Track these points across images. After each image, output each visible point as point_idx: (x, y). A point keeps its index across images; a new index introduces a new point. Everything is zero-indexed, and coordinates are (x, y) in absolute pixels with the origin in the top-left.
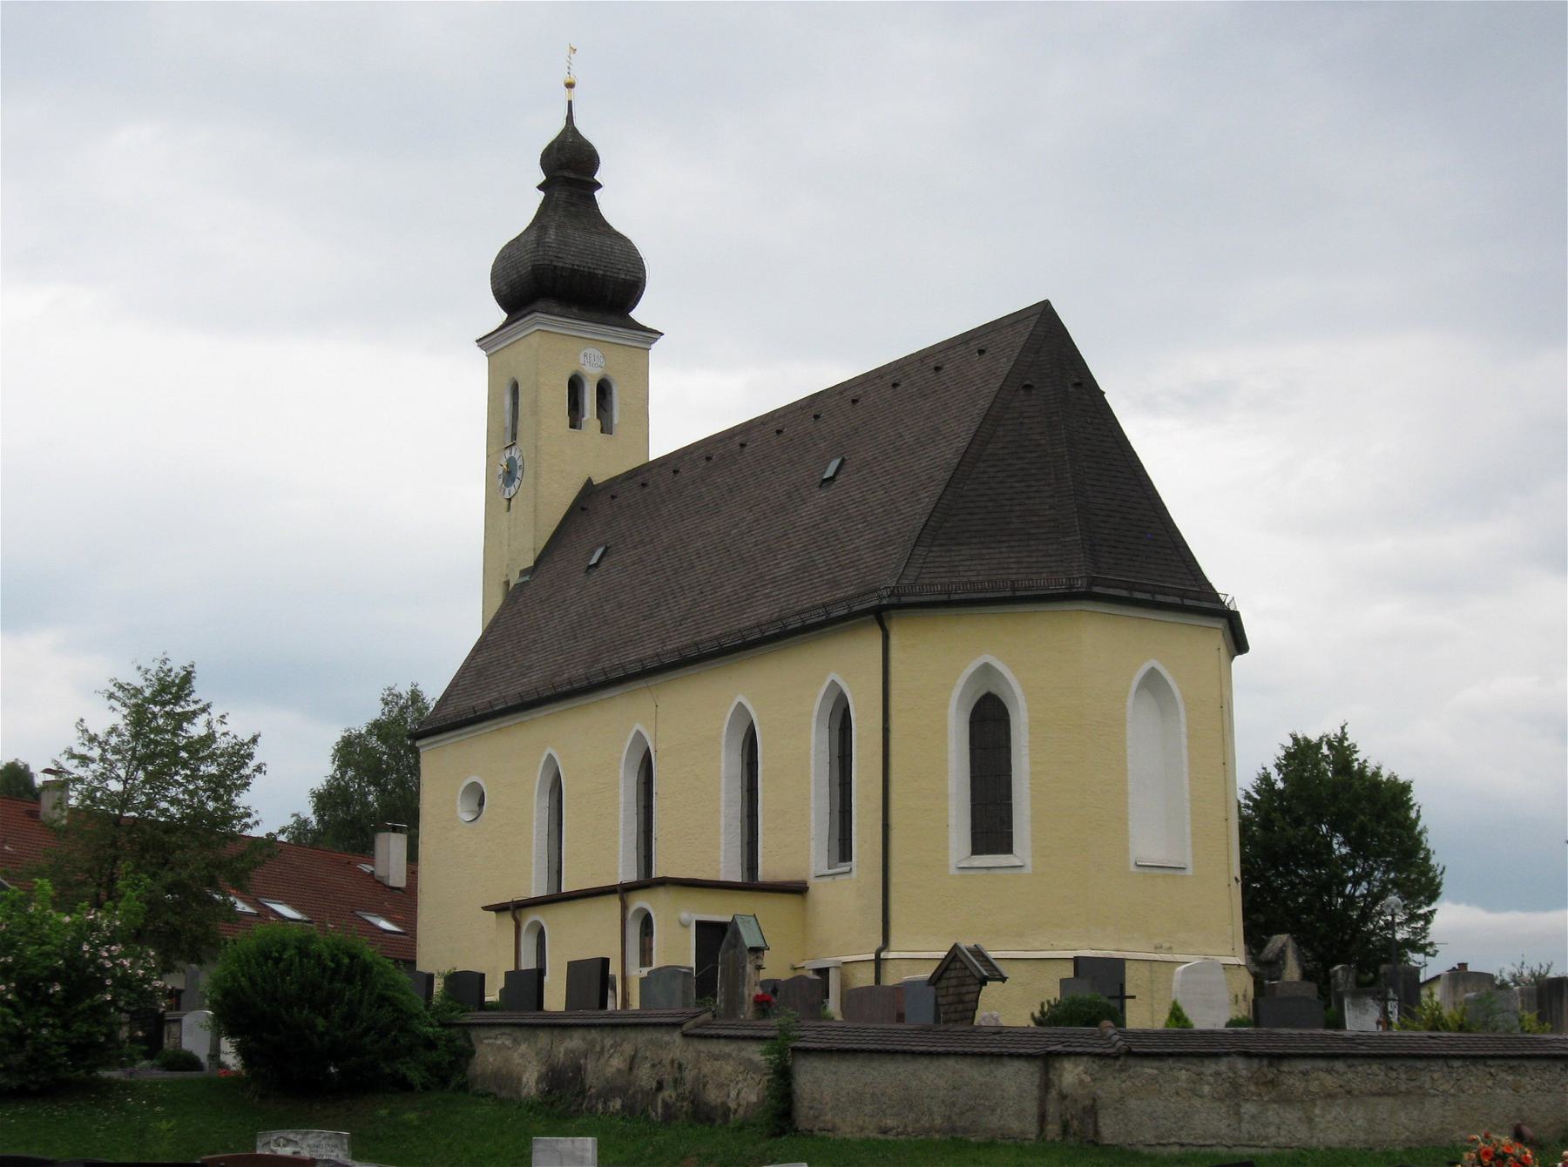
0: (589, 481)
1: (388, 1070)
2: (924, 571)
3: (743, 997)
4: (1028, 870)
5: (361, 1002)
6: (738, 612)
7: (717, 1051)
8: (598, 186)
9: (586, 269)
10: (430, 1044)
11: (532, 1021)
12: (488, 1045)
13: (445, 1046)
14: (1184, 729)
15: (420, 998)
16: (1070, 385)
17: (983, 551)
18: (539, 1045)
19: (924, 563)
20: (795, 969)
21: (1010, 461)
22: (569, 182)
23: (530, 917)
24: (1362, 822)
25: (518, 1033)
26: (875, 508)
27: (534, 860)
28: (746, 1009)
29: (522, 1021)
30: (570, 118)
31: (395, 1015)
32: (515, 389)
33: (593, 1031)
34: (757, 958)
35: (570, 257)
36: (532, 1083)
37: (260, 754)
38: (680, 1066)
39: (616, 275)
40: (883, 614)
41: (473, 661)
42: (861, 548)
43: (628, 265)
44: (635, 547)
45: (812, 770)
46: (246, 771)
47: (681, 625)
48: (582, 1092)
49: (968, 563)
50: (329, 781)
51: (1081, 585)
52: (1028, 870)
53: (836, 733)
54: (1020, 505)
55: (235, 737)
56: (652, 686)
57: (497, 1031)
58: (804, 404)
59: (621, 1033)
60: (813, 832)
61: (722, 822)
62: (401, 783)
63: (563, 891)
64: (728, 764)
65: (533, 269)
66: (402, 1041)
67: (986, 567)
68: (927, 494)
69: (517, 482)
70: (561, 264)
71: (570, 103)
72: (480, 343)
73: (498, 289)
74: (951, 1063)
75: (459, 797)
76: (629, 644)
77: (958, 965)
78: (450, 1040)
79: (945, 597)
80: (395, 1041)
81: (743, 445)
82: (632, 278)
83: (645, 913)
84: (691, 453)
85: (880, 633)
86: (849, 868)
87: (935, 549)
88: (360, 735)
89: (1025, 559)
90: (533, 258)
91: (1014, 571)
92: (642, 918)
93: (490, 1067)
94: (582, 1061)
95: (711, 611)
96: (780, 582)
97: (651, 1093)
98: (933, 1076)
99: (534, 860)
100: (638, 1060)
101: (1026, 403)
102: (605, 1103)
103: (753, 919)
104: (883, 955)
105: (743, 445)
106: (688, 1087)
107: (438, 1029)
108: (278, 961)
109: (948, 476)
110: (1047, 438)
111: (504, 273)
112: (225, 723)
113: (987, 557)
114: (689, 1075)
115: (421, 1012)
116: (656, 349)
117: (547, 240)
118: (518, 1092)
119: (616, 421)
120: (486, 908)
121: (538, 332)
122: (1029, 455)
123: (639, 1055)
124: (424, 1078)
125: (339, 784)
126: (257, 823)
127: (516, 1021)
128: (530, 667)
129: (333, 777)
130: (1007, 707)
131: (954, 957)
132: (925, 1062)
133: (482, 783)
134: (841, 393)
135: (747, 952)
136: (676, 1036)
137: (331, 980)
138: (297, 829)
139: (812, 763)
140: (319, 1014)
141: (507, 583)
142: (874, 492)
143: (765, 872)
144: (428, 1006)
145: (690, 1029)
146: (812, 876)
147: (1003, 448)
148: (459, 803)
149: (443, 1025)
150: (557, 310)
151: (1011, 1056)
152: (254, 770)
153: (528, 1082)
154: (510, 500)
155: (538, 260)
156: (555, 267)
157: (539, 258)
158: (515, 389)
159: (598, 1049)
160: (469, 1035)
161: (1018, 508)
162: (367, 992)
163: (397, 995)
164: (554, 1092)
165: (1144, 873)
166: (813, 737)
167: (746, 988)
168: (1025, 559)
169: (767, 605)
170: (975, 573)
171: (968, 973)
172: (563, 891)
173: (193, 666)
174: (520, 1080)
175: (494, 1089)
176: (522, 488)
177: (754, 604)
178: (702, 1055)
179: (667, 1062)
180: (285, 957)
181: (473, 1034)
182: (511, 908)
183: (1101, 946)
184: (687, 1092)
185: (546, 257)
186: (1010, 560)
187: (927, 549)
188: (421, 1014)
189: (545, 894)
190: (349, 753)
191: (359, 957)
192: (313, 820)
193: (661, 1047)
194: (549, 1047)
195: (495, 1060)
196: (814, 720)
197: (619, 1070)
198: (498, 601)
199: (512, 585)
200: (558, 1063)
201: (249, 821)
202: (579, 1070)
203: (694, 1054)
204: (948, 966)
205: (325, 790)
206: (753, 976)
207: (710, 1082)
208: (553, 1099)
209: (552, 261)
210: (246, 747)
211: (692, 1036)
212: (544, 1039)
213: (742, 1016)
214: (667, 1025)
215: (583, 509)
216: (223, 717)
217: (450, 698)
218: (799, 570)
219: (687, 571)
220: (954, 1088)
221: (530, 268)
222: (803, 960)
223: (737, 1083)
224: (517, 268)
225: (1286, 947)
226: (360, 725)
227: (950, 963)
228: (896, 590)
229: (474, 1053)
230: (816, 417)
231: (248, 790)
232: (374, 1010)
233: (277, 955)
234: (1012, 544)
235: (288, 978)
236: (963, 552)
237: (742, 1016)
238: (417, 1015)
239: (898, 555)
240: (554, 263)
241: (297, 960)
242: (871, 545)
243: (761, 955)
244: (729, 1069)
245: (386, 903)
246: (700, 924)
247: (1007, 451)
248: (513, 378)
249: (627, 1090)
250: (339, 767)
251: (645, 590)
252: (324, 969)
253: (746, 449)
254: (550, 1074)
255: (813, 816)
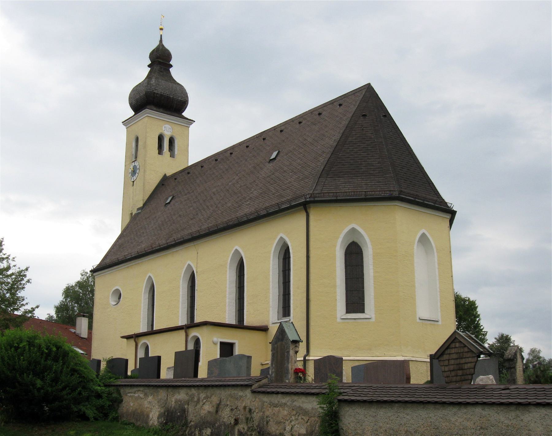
0: (165, 175)
1: (75, 410)
2: (324, 187)
3: (288, 370)
4: (373, 320)
5: (61, 372)
6: (235, 212)
7: (276, 402)
8: (171, 66)
9: (166, 95)
10: (99, 396)
11: (156, 384)
12: (130, 396)
13: (107, 396)
14: (436, 260)
15: (94, 372)
16: (381, 116)
17: (350, 180)
18: (160, 397)
19: (324, 184)
20: (262, 365)
21: (359, 144)
22: (160, 63)
23: (143, 341)
24: (461, 315)
25: (147, 390)
26: (297, 166)
27: (142, 320)
28: (290, 376)
29: (150, 384)
30: (161, 41)
31: (80, 379)
32: (137, 140)
33: (193, 390)
34: (296, 346)
35: (160, 90)
36: (155, 418)
37: (29, 275)
38: (250, 410)
39: (178, 98)
40: (307, 206)
41: (118, 242)
42: (292, 182)
43: (182, 95)
44: (186, 195)
45: (271, 276)
46: (23, 282)
47: (208, 220)
48: (186, 424)
49: (344, 185)
50: (61, 302)
51: (396, 194)
52: (373, 320)
53: (281, 260)
54: (365, 162)
55: (19, 268)
56: (196, 244)
57: (135, 389)
58: (258, 136)
59: (209, 392)
60: (271, 303)
61: (227, 301)
62: (87, 303)
63: (154, 330)
64: (230, 277)
65: (146, 93)
66: (83, 394)
67: (352, 186)
68: (322, 158)
69: (137, 174)
70: (156, 92)
71: (161, 35)
72: (124, 123)
73: (131, 102)
74: (478, 410)
75: (110, 295)
76: (185, 229)
77: (457, 345)
78: (110, 394)
79: (335, 198)
80: (80, 393)
81: (231, 154)
82: (183, 100)
83: (197, 338)
84: (209, 160)
85: (305, 214)
86: (289, 319)
87: (328, 179)
88: (72, 286)
89: (369, 184)
90: (146, 89)
91: (364, 188)
92: (194, 341)
93: (131, 408)
94: (186, 406)
95: (222, 213)
96: (254, 199)
97: (230, 425)
98: (462, 420)
99: (142, 320)
100: (221, 406)
101: (364, 122)
102: (200, 430)
103: (291, 325)
104: (307, 358)
105: (231, 154)
106: (256, 423)
107: (103, 388)
108: (17, 348)
109: (332, 150)
110: (375, 136)
111: (134, 96)
112: (14, 261)
113: (352, 182)
114: (256, 416)
115: (94, 379)
116: (192, 127)
117: (151, 82)
118: (147, 423)
119: (176, 153)
120: (123, 337)
121: (147, 117)
122: (367, 142)
123: (223, 403)
124: (95, 414)
125: (64, 304)
126: (27, 304)
127: (147, 384)
128: (142, 242)
129: (62, 301)
130: (362, 248)
131: (454, 340)
132: (455, 409)
133: (120, 289)
134: (275, 130)
135: (290, 343)
136: (248, 392)
137: (46, 360)
138: (49, 319)
139: (271, 273)
140: (39, 378)
141: (132, 214)
142: (295, 161)
143: (247, 321)
144: (97, 376)
145: (256, 389)
146: (270, 323)
147: (356, 139)
148: (110, 297)
149: (106, 386)
150: (155, 109)
151: (538, 405)
152: (26, 282)
153: (153, 418)
154: (133, 182)
155: (148, 90)
156: (154, 92)
157: (148, 89)
158: (137, 140)
159: (196, 399)
160: (120, 391)
161: (364, 163)
162: (65, 366)
163: (81, 369)
164: (168, 424)
165: (423, 323)
166: (271, 262)
167: (290, 364)
168: (369, 184)
169: (249, 208)
170: (347, 189)
171: (466, 349)
172: (154, 330)
173: (3, 239)
174: (148, 416)
175: (133, 421)
176: (139, 177)
177: (242, 209)
178: (265, 404)
179: (241, 408)
180: (21, 346)
181: (122, 391)
182: (134, 337)
183: (406, 355)
184: (255, 426)
185: (151, 89)
186: (363, 184)
187: (325, 179)
188: (94, 380)
189: (146, 331)
190: (69, 292)
191: (61, 348)
192: (55, 316)
193: (237, 399)
194: (166, 398)
195: (134, 405)
196: (272, 254)
197: (209, 412)
198: (128, 220)
199: (133, 214)
200: (171, 407)
201: (24, 302)
202: (184, 411)
203: (260, 403)
204: (449, 345)
205: (59, 305)
206: (293, 357)
207: (271, 420)
208: (168, 428)
209: (153, 90)
210: (23, 272)
211: (259, 392)
212: (162, 394)
213: (287, 381)
214: (242, 385)
215: (163, 185)
216: (14, 258)
217: (108, 256)
218: (262, 193)
219: (209, 200)
220: (481, 428)
221: (145, 93)
222: (266, 361)
223: (291, 422)
224: (139, 93)
225: (517, 352)
226: (73, 282)
227: (451, 344)
228: (313, 195)
229: (122, 401)
230: (264, 139)
231: (24, 290)
232: (69, 376)
233: (17, 345)
234: (363, 177)
235: (22, 357)
236: (341, 180)
237: (287, 381)
238: (92, 380)
239: (311, 182)
240: (154, 91)
241: (27, 347)
242: (297, 180)
243: (298, 345)
244: (286, 413)
245: (80, 343)
246: (222, 344)
247: (357, 140)
248: (136, 135)
249: (215, 424)
250: (65, 297)
251: (191, 209)
252: (42, 353)
253: (232, 155)
254: (166, 413)
255: (271, 297)
